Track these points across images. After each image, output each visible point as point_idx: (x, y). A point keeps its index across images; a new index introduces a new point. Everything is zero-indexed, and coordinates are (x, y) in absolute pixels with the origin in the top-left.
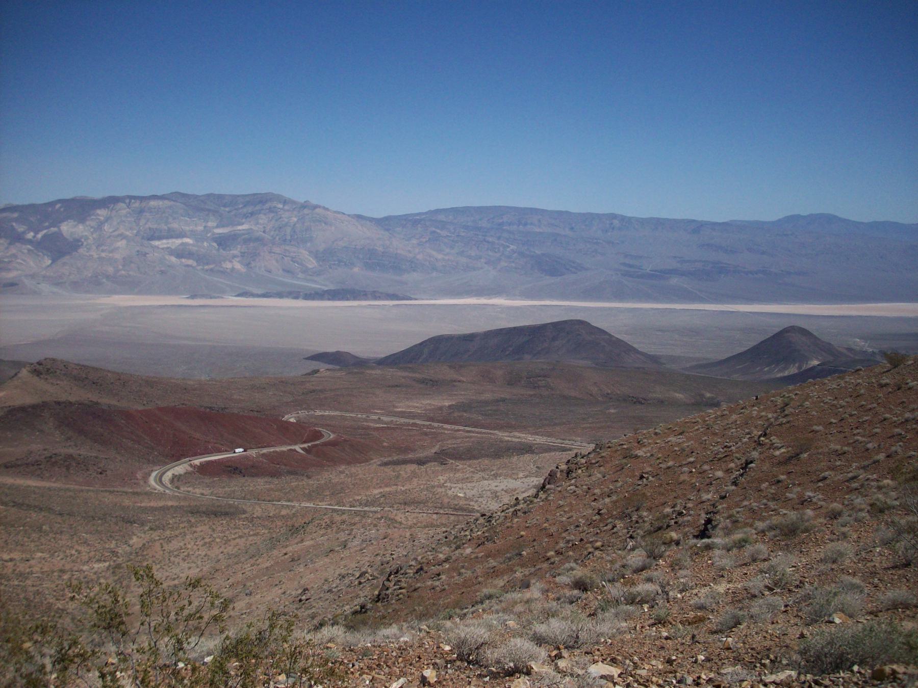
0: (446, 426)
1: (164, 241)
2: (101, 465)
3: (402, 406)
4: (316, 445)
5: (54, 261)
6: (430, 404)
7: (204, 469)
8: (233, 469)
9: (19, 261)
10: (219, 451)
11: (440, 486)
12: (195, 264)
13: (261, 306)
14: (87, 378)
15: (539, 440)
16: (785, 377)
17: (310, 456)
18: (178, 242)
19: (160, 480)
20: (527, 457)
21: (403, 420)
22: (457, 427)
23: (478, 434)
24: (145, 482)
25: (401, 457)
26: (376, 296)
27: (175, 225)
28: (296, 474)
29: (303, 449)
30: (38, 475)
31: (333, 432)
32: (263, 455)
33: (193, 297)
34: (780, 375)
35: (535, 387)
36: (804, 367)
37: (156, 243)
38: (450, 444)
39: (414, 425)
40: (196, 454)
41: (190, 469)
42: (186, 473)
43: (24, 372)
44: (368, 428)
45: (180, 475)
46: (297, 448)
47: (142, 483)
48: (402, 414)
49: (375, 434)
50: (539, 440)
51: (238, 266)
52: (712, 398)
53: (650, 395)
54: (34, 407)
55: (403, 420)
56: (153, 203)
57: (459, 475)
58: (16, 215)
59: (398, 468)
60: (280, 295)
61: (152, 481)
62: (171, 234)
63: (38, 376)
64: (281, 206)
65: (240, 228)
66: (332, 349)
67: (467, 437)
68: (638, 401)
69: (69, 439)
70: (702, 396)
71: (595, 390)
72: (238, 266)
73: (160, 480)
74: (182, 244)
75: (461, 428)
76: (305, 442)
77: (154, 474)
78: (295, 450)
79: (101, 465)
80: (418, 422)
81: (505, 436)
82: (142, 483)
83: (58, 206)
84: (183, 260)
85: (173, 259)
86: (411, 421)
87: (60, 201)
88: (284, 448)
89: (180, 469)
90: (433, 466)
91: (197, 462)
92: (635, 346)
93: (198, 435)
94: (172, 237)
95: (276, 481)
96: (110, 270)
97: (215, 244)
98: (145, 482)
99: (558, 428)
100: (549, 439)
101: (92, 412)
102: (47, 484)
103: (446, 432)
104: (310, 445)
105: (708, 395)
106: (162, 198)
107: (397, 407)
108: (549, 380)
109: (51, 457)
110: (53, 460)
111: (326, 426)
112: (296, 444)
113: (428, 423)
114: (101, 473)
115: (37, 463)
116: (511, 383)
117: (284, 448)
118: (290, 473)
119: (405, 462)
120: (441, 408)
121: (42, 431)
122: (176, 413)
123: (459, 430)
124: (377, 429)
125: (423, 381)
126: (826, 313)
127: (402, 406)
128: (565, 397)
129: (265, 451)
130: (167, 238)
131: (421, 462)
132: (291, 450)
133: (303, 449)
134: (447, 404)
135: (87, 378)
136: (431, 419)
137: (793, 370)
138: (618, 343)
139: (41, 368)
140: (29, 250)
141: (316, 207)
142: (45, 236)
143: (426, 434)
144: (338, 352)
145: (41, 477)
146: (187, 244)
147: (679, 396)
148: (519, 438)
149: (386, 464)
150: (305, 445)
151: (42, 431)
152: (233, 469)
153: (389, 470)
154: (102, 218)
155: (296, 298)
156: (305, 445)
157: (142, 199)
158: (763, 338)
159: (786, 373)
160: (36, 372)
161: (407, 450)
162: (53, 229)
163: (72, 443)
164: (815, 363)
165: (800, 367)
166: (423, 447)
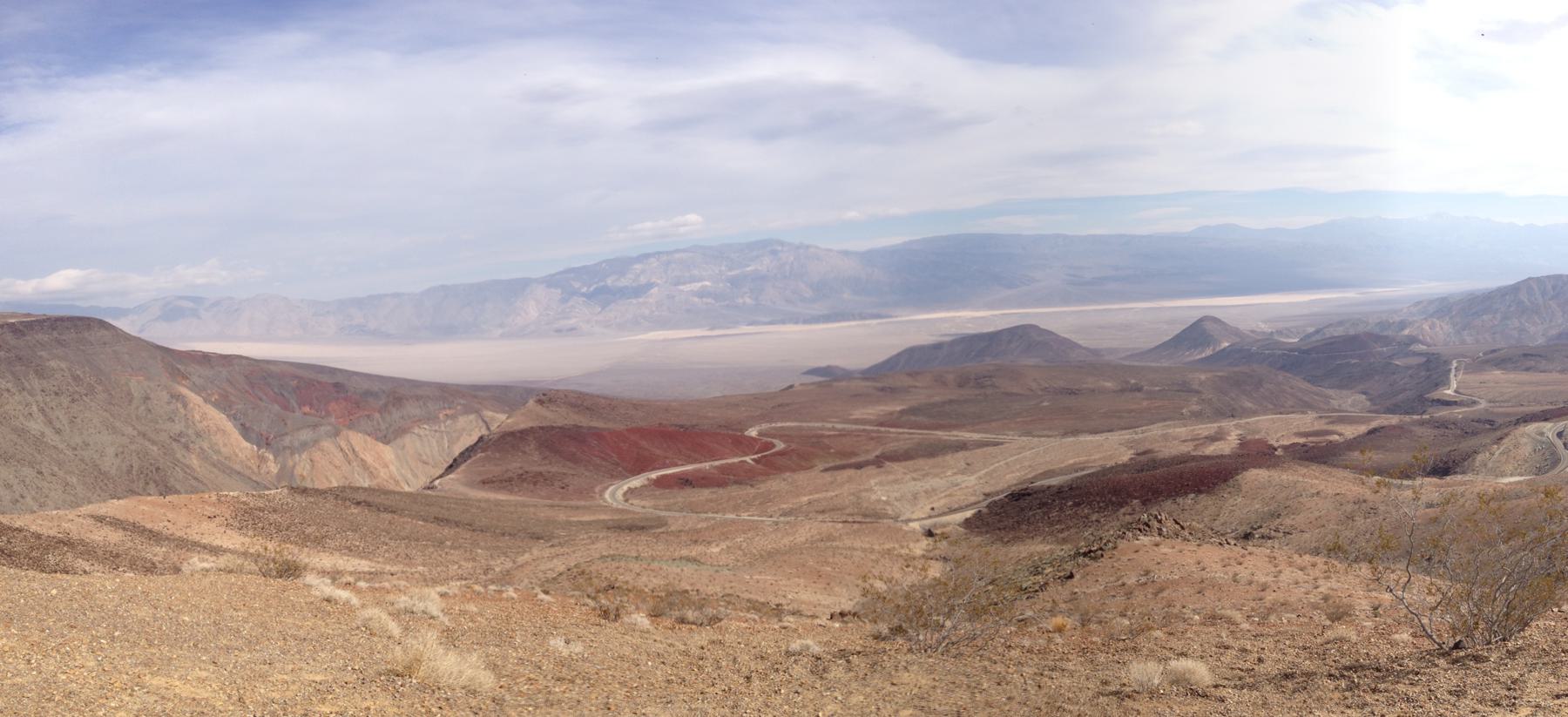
0: (892, 430)
1: (688, 285)
2: (566, 481)
3: (858, 413)
4: (765, 456)
5: (603, 308)
6: (882, 411)
7: (661, 483)
8: (685, 482)
9: (577, 310)
10: (676, 465)
11: (866, 490)
12: (713, 302)
13: (1233, 306)
14: (582, 405)
15: (976, 436)
16: (1202, 359)
17: (760, 466)
18: (700, 284)
19: (613, 495)
20: (961, 454)
21: (854, 427)
22: (901, 430)
23: (919, 435)
24: (601, 495)
25: (844, 462)
26: (862, 317)
27: (696, 272)
28: (741, 484)
29: (753, 460)
30: (509, 490)
31: (785, 442)
32: (716, 467)
33: (712, 329)
34: (1199, 357)
35: (982, 387)
36: (1218, 349)
37: (681, 287)
38: (891, 447)
39: (864, 430)
40: (654, 469)
41: (646, 482)
42: (642, 486)
43: (531, 402)
44: (822, 436)
45: (636, 488)
46: (748, 459)
47: (597, 496)
48: (856, 422)
49: (826, 441)
50: (976, 436)
51: (748, 300)
52: (1136, 384)
53: (1085, 386)
54: (522, 432)
55: (854, 427)
56: (677, 256)
57: (891, 477)
58: (572, 275)
59: (836, 473)
60: (783, 322)
61: (607, 495)
62: (693, 280)
63: (541, 404)
64: (780, 248)
65: (749, 269)
66: (823, 364)
67: (908, 439)
68: (1073, 393)
69: (545, 458)
70: (1128, 382)
71: (1034, 386)
72: (748, 300)
73: (613, 495)
74: (702, 286)
75: (906, 430)
76: (756, 453)
77: (611, 488)
78: (745, 462)
79: (566, 481)
80: (868, 427)
81: (941, 434)
82: (597, 496)
83: (604, 265)
84: (704, 300)
85: (696, 299)
86: (862, 427)
87: (604, 261)
88: (736, 460)
89: (636, 482)
90: (871, 470)
91: (654, 475)
92: (1080, 342)
93: (658, 452)
94: (694, 281)
95: (721, 491)
96: (647, 312)
97: (729, 284)
98: (601, 495)
99: (994, 424)
100: (984, 435)
101: (575, 435)
102: (512, 498)
103: (892, 435)
104: (759, 455)
105: (1133, 381)
106: (684, 251)
107: (851, 415)
108: (994, 379)
109: (522, 475)
110: (524, 477)
111: (774, 437)
112: (747, 455)
113: (876, 428)
114: (563, 488)
115: (510, 480)
116: (960, 386)
117: (736, 460)
118: (736, 482)
119: (843, 467)
120: (891, 413)
121: (524, 452)
122: (642, 432)
123: (903, 433)
124: (829, 436)
125: (883, 389)
126: (693, 335)
127: (858, 413)
128: (1007, 394)
129: (717, 463)
130: (690, 282)
131: (859, 466)
132: (742, 461)
133: (753, 460)
134: (898, 408)
135: (582, 405)
136: (881, 424)
137: (1209, 352)
138: (1065, 341)
139: (543, 397)
140: (584, 301)
141: (808, 247)
142: (596, 289)
143: (872, 439)
144: (829, 367)
145: (511, 492)
146: (706, 286)
147: (1108, 384)
148: (957, 436)
149: (826, 470)
150: (756, 456)
151: (524, 452)
152: (685, 482)
153: (828, 477)
154: (638, 271)
155: (796, 323)
156: (756, 456)
157: (668, 253)
158: (1184, 327)
159: (1203, 355)
160: (540, 402)
161: (854, 454)
162: (603, 284)
163: (547, 462)
164: (1227, 344)
165: (1214, 349)
166: (867, 451)
